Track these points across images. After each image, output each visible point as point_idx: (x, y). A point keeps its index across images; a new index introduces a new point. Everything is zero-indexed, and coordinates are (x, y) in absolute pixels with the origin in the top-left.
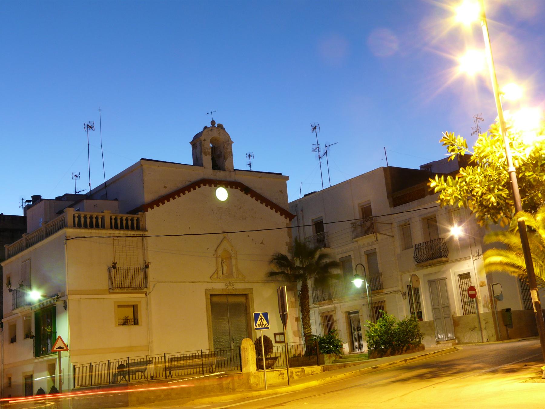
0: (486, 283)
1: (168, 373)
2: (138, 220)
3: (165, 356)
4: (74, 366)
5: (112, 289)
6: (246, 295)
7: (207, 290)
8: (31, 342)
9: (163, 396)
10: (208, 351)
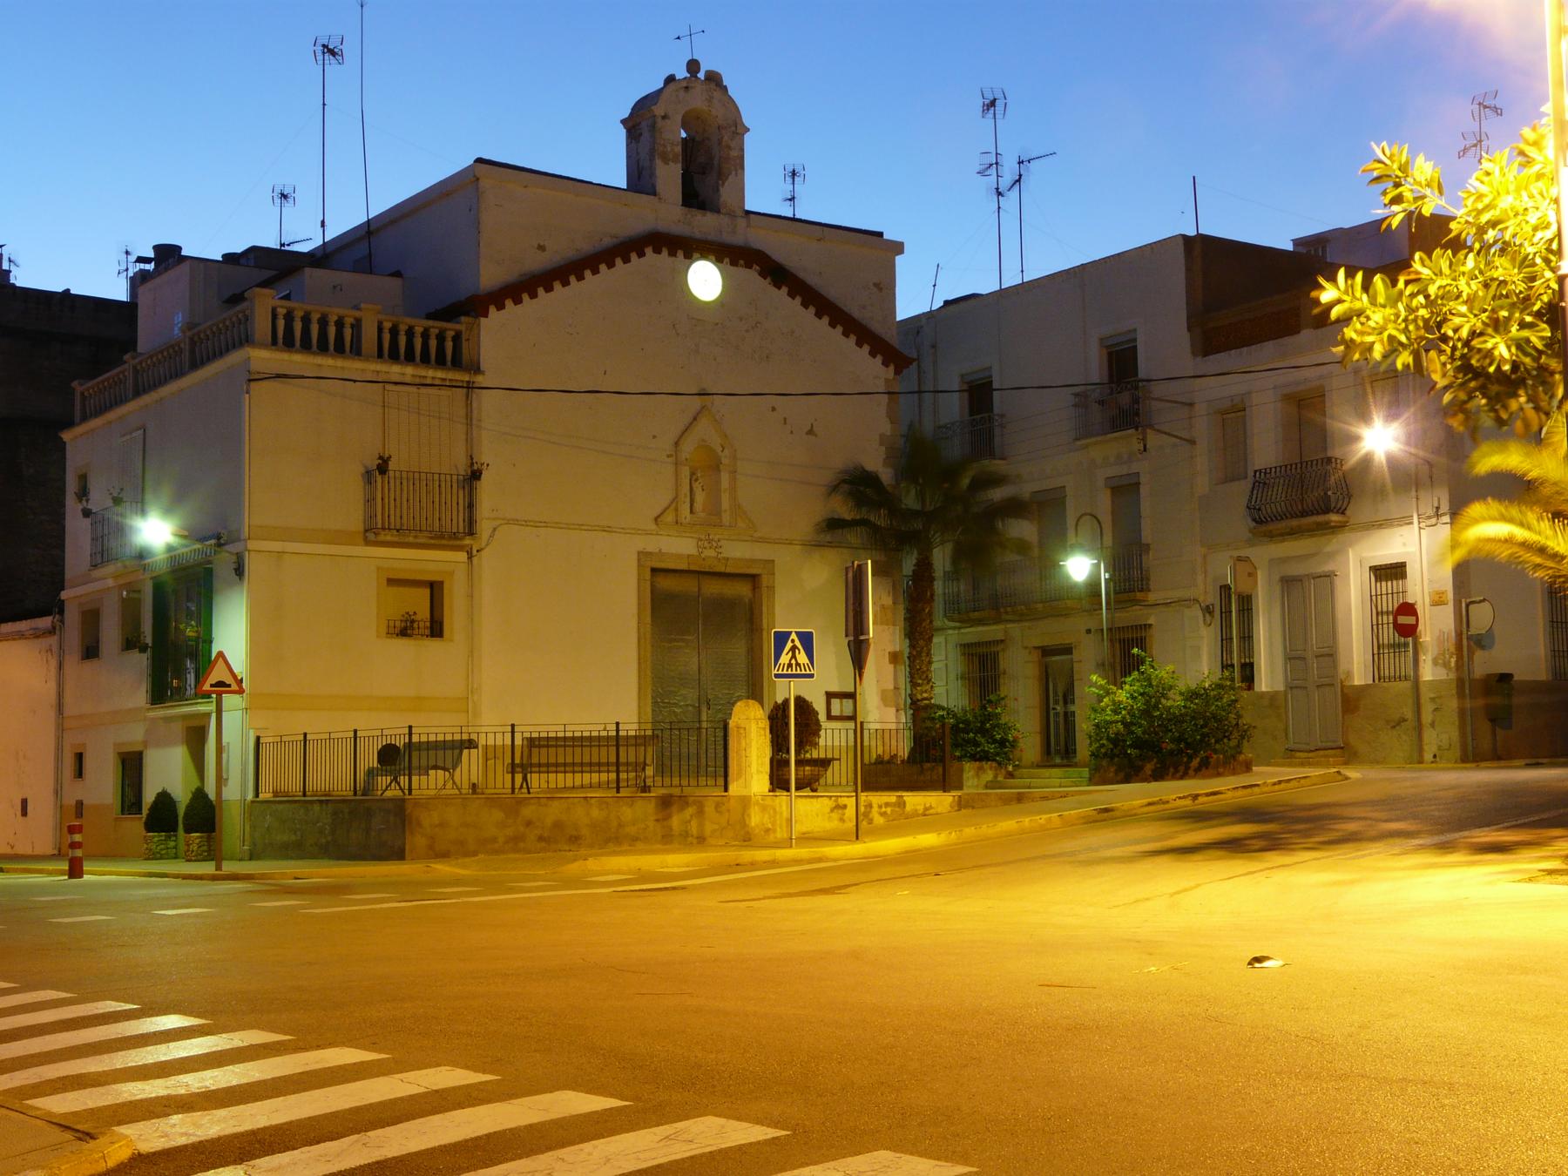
0: (1450, 596)
1: (519, 778)
2: (457, 338)
3: (513, 732)
4: (258, 738)
5: (371, 533)
6: (753, 579)
7: (642, 555)
8: (140, 662)
9: (501, 840)
10: (635, 726)
